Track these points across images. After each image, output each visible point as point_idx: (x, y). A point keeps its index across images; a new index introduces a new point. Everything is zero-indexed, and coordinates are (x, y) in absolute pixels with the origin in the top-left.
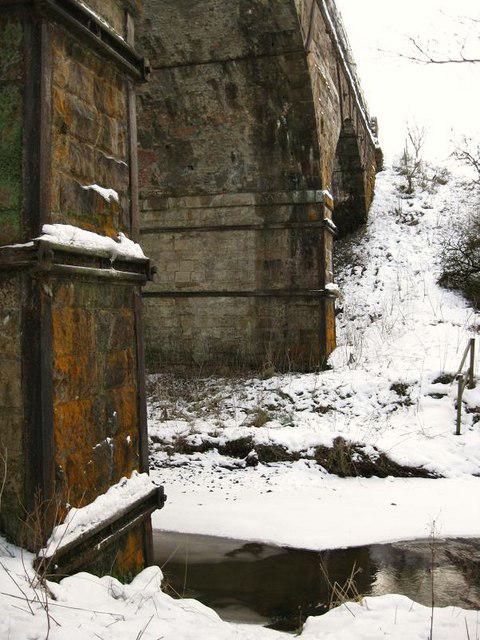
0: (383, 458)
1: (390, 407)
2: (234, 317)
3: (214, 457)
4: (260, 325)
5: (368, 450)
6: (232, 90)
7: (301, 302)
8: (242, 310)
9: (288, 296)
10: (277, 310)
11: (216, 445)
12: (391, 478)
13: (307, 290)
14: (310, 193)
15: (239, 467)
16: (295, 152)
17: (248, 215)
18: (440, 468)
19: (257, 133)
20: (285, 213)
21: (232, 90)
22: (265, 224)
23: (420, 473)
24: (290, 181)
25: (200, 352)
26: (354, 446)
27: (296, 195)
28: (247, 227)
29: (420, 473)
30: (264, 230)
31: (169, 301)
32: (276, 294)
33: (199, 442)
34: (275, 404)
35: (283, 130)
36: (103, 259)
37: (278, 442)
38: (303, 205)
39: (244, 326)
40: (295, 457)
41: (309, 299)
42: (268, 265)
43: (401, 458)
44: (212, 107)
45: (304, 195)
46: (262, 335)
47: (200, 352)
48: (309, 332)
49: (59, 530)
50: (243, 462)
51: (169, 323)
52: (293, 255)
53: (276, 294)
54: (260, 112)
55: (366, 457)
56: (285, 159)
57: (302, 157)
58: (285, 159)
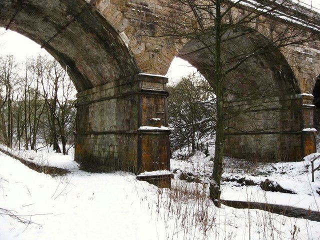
0: (279, 186)
1: (301, 173)
2: (273, 141)
3: (235, 183)
4: (282, 144)
5: (274, 183)
6: (262, 64)
7: (294, 136)
8: (276, 139)
9: (290, 133)
10: (287, 138)
11: (236, 180)
12: (278, 192)
13: (296, 131)
14: (296, 95)
15: (239, 186)
16: (290, 81)
17: (278, 104)
18: (296, 190)
19: (274, 76)
20: (288, 103)
21: (262, 64)
22: (282, 108)
23: (290, 192)
24: (290, 91)
25: (263, 154)
26: (270, 182)
27: (292, 96)
28: (277, 109)
29: (290, 192)
30: (282, 110)
31: (254, 136)
32: (286, 133)
33: (231, 178)
34: (271, 171)
35: (283, 74)
36: (155, 131)
37: (252, 180)
38: (295, 100)
39: (276, 144)
40: (256, 184)
41: (297, 134)
42: (284, 122)
43: (284, 187)
44: (258, 69)
45: (294, 96)
46: (282, 148)
47: (263, 154)
48: (297, 147)
49: (141, 174)
50: (241, 185)
51: (253, 144)
52: (292, 118)
53: (286, 133)
54: (273, 69)
55: (273, 185)
56: (286, 84)
57: (292, 83)
58: (286, 84)
